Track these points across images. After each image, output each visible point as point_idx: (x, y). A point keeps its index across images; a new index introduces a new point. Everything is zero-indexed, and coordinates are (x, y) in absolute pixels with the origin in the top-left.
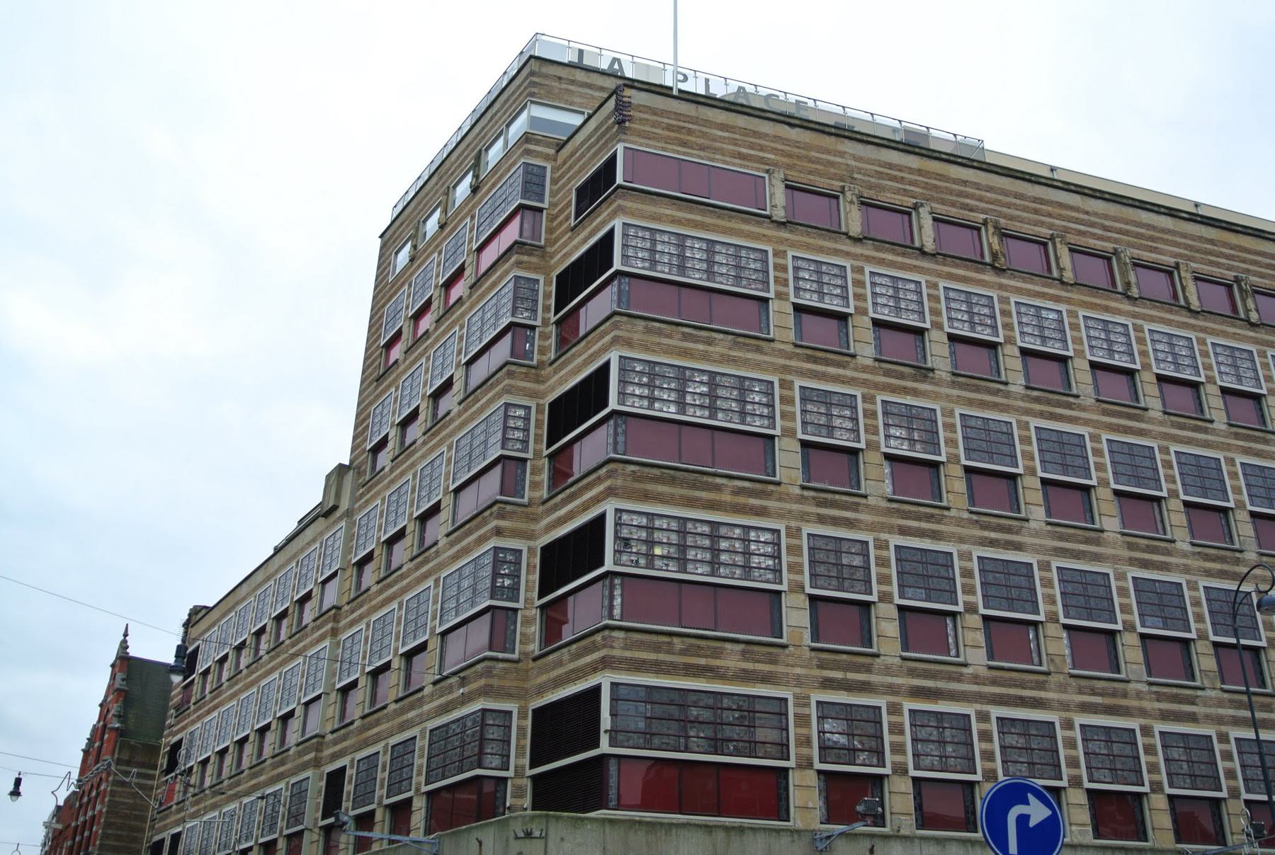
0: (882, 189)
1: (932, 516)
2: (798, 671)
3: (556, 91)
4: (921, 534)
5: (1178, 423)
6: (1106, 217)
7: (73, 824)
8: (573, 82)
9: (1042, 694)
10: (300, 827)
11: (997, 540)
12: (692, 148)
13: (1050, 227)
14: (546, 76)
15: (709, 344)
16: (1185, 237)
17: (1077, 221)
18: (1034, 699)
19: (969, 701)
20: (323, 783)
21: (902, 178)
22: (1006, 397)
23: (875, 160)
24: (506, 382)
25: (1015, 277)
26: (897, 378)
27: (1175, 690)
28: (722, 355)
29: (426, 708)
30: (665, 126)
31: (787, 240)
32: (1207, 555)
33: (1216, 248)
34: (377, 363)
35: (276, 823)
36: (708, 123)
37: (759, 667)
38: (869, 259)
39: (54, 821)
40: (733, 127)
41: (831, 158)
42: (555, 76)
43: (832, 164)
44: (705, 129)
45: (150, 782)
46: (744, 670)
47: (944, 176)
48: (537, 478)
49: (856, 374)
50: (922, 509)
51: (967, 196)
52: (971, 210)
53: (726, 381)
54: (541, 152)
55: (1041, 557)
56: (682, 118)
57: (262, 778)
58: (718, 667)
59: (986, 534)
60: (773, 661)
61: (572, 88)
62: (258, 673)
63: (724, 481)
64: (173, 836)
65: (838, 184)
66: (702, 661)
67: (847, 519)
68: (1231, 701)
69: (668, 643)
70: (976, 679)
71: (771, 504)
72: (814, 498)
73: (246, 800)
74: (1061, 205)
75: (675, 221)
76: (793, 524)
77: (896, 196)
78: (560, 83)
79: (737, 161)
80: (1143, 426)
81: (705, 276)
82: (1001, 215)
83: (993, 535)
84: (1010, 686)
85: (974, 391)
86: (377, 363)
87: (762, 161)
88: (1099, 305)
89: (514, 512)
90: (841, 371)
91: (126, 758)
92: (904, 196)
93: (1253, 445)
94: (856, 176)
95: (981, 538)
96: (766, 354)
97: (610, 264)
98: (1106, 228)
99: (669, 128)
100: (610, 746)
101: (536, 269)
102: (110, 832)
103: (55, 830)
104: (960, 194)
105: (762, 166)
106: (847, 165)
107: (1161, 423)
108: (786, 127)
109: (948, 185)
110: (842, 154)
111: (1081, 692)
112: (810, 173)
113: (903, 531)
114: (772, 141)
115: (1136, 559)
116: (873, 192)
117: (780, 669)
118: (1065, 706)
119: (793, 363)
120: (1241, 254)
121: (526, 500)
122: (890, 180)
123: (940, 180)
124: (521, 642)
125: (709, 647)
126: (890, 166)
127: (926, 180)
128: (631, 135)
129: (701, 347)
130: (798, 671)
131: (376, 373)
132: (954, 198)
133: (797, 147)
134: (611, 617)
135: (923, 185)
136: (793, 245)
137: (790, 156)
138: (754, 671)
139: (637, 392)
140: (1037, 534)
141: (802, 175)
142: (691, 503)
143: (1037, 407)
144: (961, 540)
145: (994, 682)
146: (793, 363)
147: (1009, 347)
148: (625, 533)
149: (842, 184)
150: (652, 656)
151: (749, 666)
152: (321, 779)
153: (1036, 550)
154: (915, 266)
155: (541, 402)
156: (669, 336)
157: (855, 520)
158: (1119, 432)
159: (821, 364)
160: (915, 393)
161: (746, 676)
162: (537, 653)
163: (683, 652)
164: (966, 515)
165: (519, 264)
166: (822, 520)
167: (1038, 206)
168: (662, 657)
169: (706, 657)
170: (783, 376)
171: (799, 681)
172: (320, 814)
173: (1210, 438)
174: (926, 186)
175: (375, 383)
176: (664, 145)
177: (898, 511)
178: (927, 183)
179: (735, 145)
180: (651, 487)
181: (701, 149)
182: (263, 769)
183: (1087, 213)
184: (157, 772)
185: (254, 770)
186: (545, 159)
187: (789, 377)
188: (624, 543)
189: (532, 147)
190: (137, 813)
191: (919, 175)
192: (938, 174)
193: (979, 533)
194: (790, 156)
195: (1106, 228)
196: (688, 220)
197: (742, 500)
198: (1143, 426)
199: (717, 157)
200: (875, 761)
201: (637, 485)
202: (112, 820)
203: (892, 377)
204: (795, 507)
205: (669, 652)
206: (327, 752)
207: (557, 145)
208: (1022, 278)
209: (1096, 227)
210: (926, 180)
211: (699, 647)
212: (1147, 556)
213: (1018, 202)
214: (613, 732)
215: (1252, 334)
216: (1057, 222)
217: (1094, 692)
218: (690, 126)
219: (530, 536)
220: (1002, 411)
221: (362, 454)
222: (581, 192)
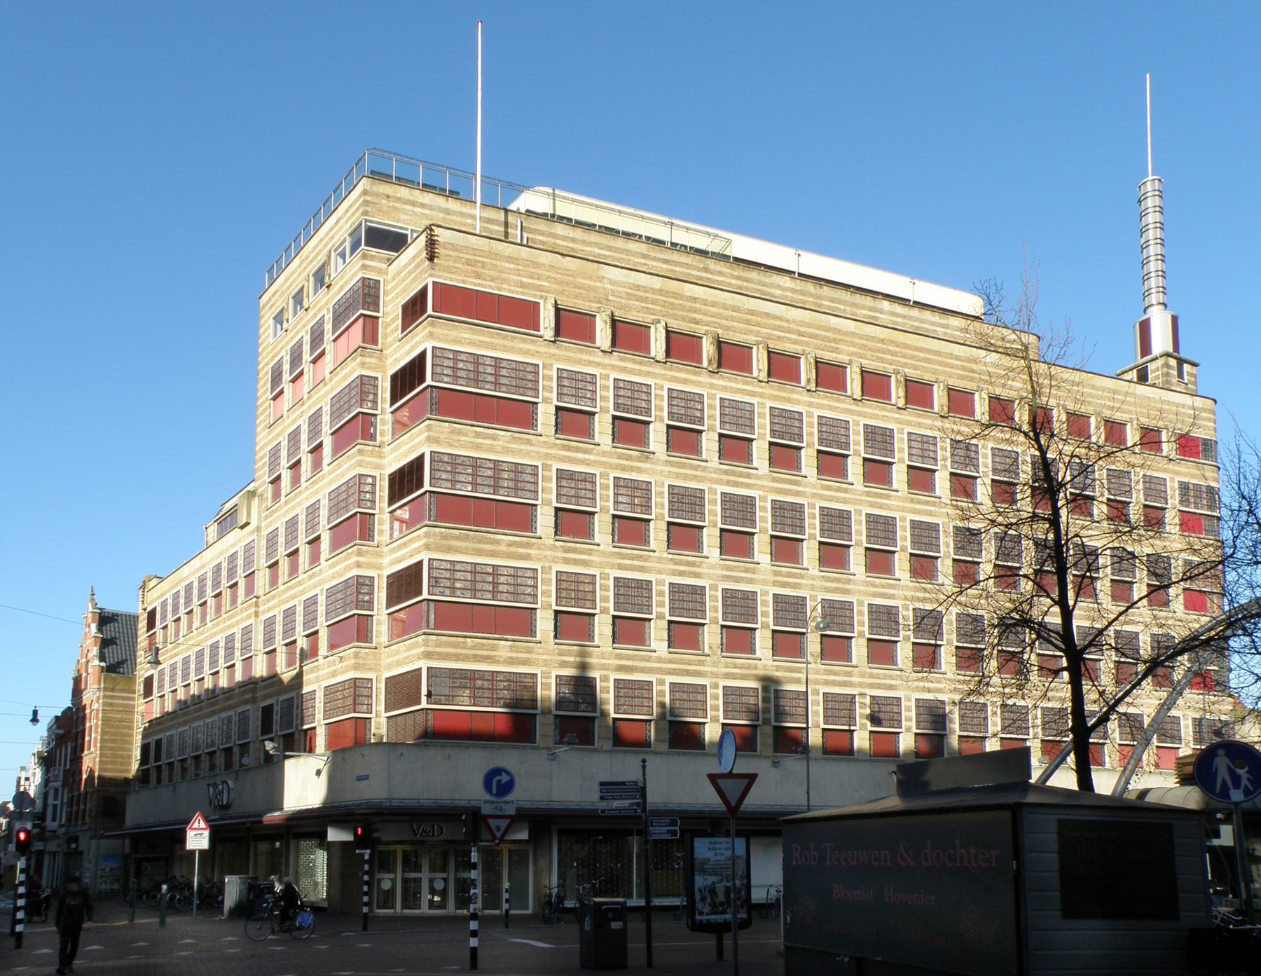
0: (630, 308)
1: (642, 556)
2: (545, 657)
3: (385, 209)
4: (633, 568)
5: (826, 486)
6: (802, 323)
7: (74, 731)
8: (398, 200)
9: (702, 668)
10: (248, 740)
11: (684, 572)
12: (484, 279)
13: (758, 334)
14: (377, 195)
15: (494, 440)
16: (862, 338)
17: (779, 329)
18: (696, 671)
19: (653, 673)
20: (260, 713)
21: (647, 298)
22: (704, 471)
23: (627, 283)
24: (358, 458)
25: (723, 377)
26: (627, 460)
27: (789, 664)
28: (503, 447)
29: (321, 673)
30: (464, 260)
31: (554, 355)
32: (828, 577)
33: (884, 346)
34: (267, 412)
35: (231, 737)
36: (497, 256)
37: (521, 655)
38: (613, 367)
39: (55, 727)
40: (517, 259)
41: (592, 283)
42: (384, 194)
43: (593, 289)
44: (494, 262)
45: (131, 703)
46: (511, 657)
47: (680, 295)
48: (382, 527)
49: (597, 458)
50: (635, 552)
51: (695, 311)
52: (697, 323)
53: (505, 467)
54: (376, 267)
55: (712, 582)
56: (478, 253)
57: (217, 707)
58: (495, 656)
59: (677, 567)
60: (530, 652)
61: (397, 205)
62: (205, 635)
63: (502, 537)
64: (156, 741)
65: (595, 305)
66: (485, 653)
67: (584, 560)
68: (825, 670)
69: (464, 643)
70: (659, 660)
71: (532, 552)
72: (562, 547)
73: (208, 720)
74: (768, 315)
75: (471, 343)
76: (547, 565)
77: (640, 314)
78: (389, 201)
79: (519, 289)
80: (800, 489)
81: (493, 388)
82: (720, 326)
83: (682, 568)
84: (681, 664)
85: (680, 468)
86: (267, 412)
87: (539, 288)
88: (784, 397)
89: (368, 551)
90: (587, 456)
91: (111, 686)
92: (646, 313)
93: (878, 500)
94: (610, 298)
95: (673, 570)
96: (534, 445)
97: (422, 380)
98: (800, 334)
99: (468, 262)
100: (428, 703)
101: (375, 368)
102: (106, 737)
103: (57, 735)
104: (691, 310)
105: (539, 293)
106: (605, 288)
107: (814, 486)
108: (559, 256)
109: (681, 302)
110: (601, 279)
111: (727, 666)
112: (576, 297)
113: (621, 567)
114: (548, 271)
115: (777, 582)
116: (622, 311)
117: (534, 656)
118: (715, 675)
119: (553, 452)
120: (904, 350)
121: (376, 542)
122: (637, 300)
123: (675, 298)
124: (376, 636)
125: (489, 644)
126: (638, 288)
127: (665, 299)
128: (439, 270)
129: (488, 442)
130: (545, 657)
131: (267, 422)
132: (685, 314)
133: (567, 275)
134: (428, 627)
135: (662, 303)
136: (558, 359)
137: (560, 283)
138: (517, 658)
139: (444, 477)
140: (712, 567)
141: (569, 300)
142: (479, 552)
143: (725, 477)
144: (660, 572)
145: (671, 661)
146: (553, 452)
147: (711, 433)
148: (435, 574)
149: (599, 305)
150: (453, 651)
151: (515, 655)
152: (258, 711)
153: (709, 576)
154: (648, 372)
155: (383, 472)
156: (466, 435)
157: (589, 561)
158: (782, 493)
159: (573, 451)
160: (639, 470)
161: (511, 661)
162: (387, 644)
163: (473, 648)
164: (665, 555)
165: (363, 364)
166: (566, 561)
167: (749, 317)
168: (460, 651)
169: (487, 650)
170: (545, 462)
171: (546, 663)
172: (259, 733)
173: (847, 496)
174: (665, 303)
175: (268, 430)
176: (464, 278)
177: (619, 553)
178: (665, 302)
179: (519, 275)
180: (453, 543)
181: (491, 281)
182: (218, 701)
183: (788, 321)
184: (136, 696)
185: (211, 701)
186: (379, 273)
187: (549, 462)
188: (434, 581)
189: (368, 262)
190: (125, 724)
191: (660, 295)
192: (674, 293)
193: (672, 567)
194: (560, 283)
195: (800, 334)
196: (480, 341)
197: (513, 549)
198: (800, 489)
199: (504, 286)
200: (590, 709)
201: (444, 542)
202: (107, 730)
203: (623, 459)
204: (549, 553)
205: (465, 648)
206: (260, 694)
207: (388, 260)
208: (729, 378)
209: (792, 333)
210: (665, 299)
211: (482, 644)
212: (786, 579)
213: (735, 314)
214: (429, 695)
215: (897, 416)
216: (763, 330)
217: (735, 667)
218: (484, 260)
219: (379, 567)
220: (699, 481)
221: (266, 402)
222: (405, 308)
